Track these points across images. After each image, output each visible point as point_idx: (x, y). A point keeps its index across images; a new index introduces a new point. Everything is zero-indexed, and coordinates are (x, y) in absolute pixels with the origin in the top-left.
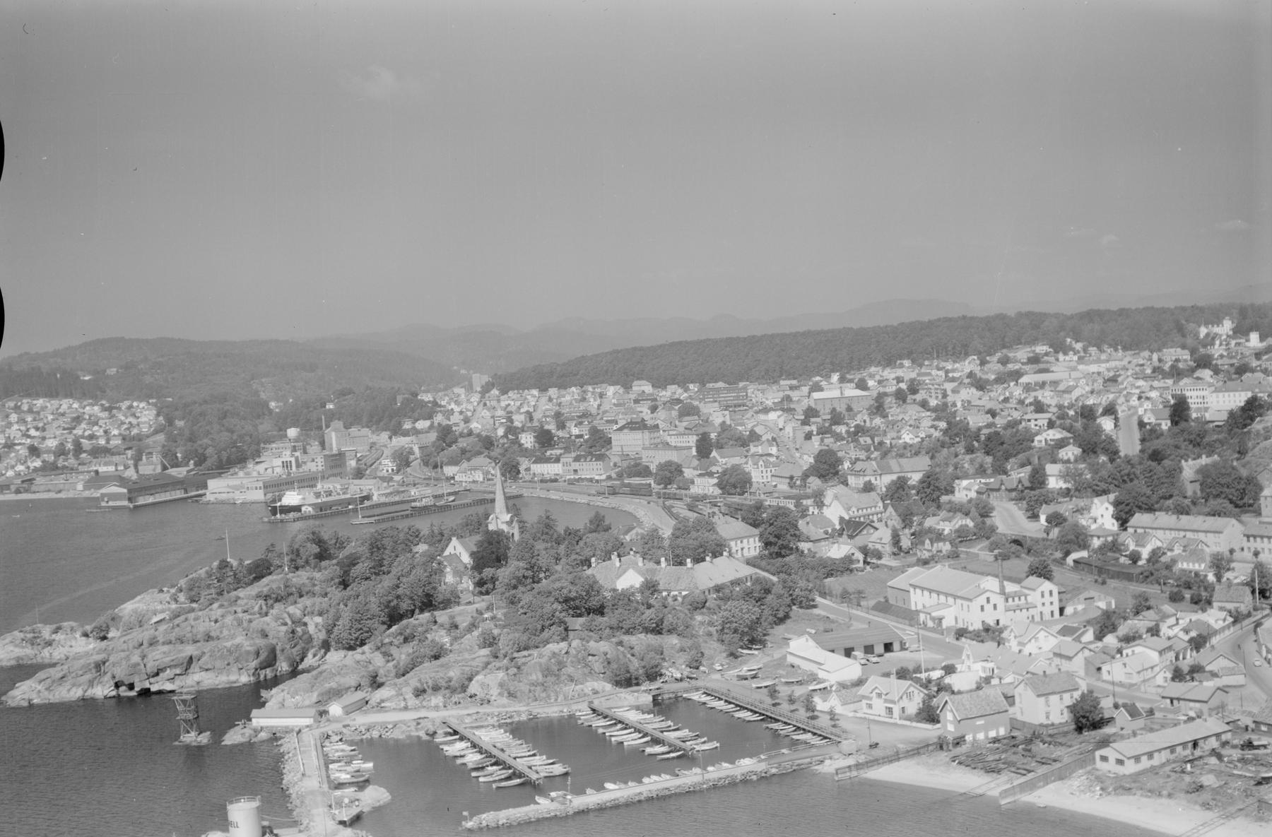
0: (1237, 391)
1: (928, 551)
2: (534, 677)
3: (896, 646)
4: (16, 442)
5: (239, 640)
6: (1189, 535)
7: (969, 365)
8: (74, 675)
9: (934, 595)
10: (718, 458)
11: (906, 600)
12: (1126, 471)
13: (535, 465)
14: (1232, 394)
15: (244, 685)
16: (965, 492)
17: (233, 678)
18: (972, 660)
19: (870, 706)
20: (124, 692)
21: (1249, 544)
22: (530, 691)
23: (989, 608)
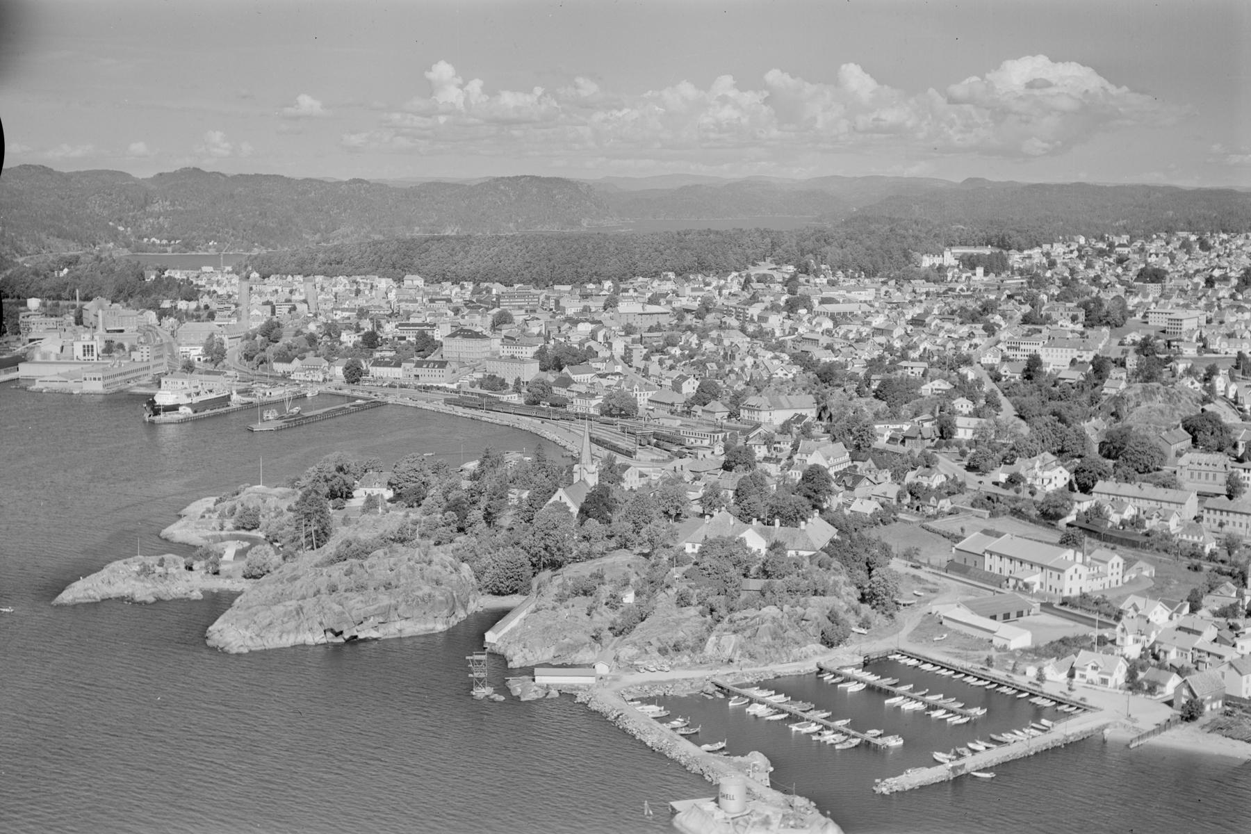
1: (934, 507)
3: (1025, 613)
6: (1165, 505)
10: (570, 374)
13: (374, 368)
14: (1059, 349)
17: (430, 626)
21: (1215, 517)
23: (1076, 577)
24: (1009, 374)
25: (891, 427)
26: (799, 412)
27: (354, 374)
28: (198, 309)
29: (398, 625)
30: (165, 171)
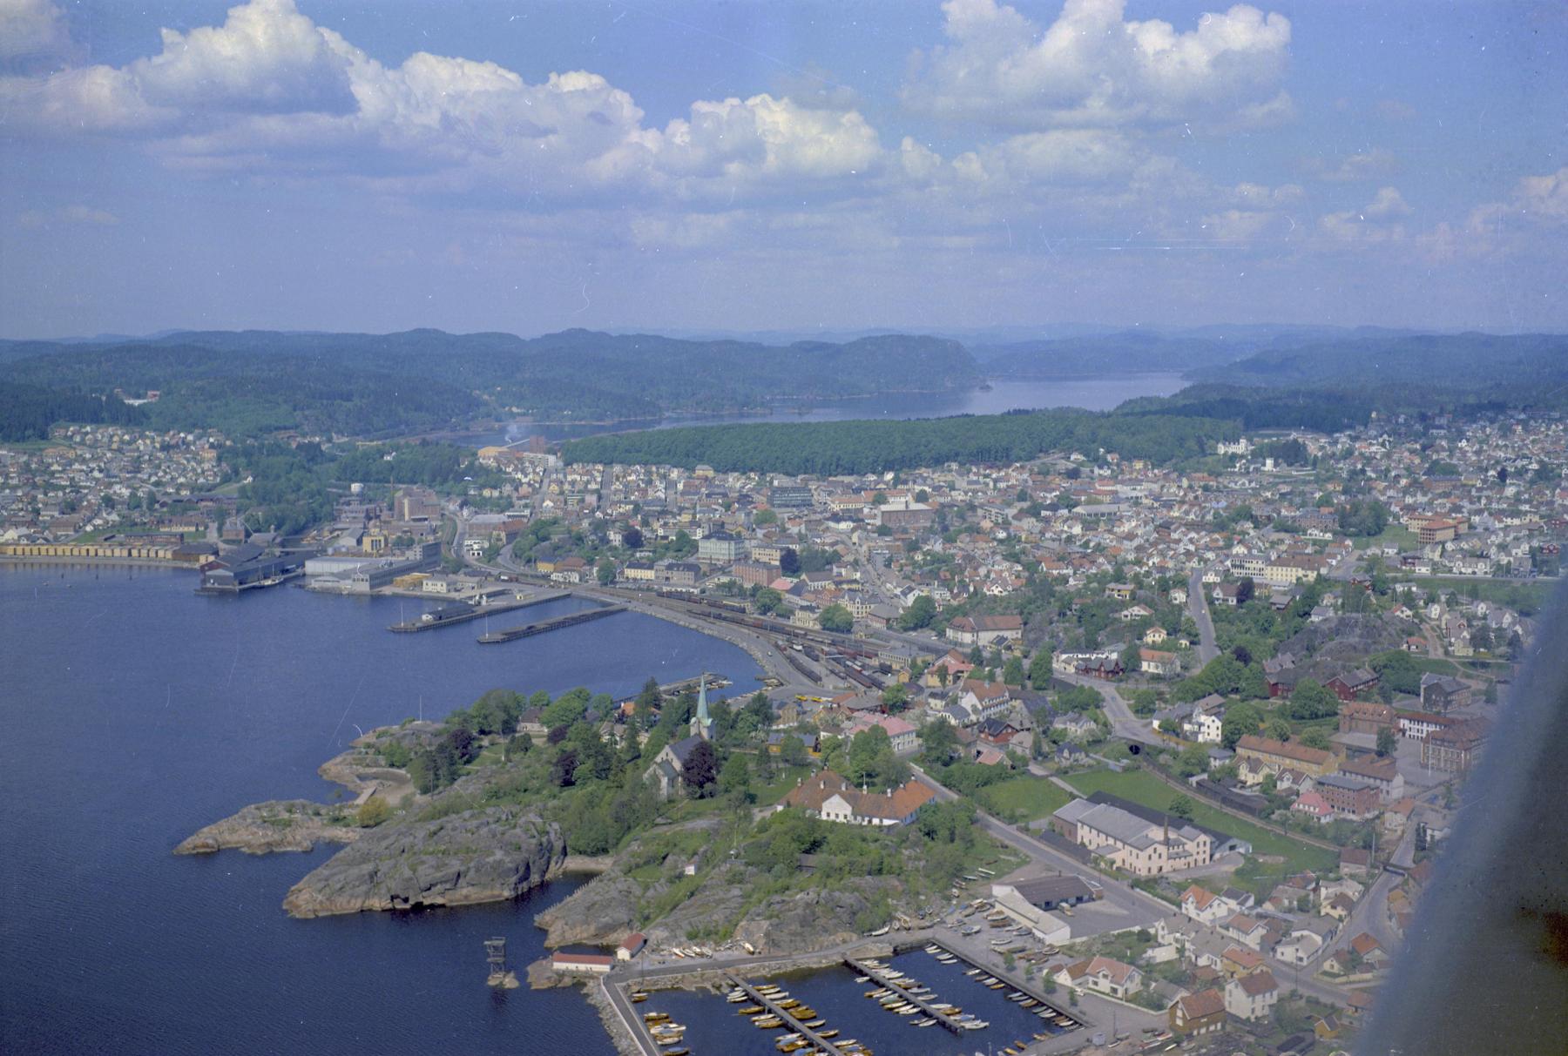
0: (1289, 566)
2: (793, 927)
4: (554, 871)
5: (499, 855)
7: (1015, 476)
8: (351, 886)
9: (1103, 836)
11: (1073, 833)
12: (1219, 672)
14: (1284, 569)
15: (507, 899)
16: (1063, 665)
17: (496, 892)
18: (1166, 932)
19: (1096, 983)
20: (400, 906)
22: (791, 941)
23: (1155, 857)
24: (1221, 596)
25: (1080, 656)
26: (1001, 633)
27: (608, 578)
28: (501, 498)
29: (464, 891)
30: (588, 328)
